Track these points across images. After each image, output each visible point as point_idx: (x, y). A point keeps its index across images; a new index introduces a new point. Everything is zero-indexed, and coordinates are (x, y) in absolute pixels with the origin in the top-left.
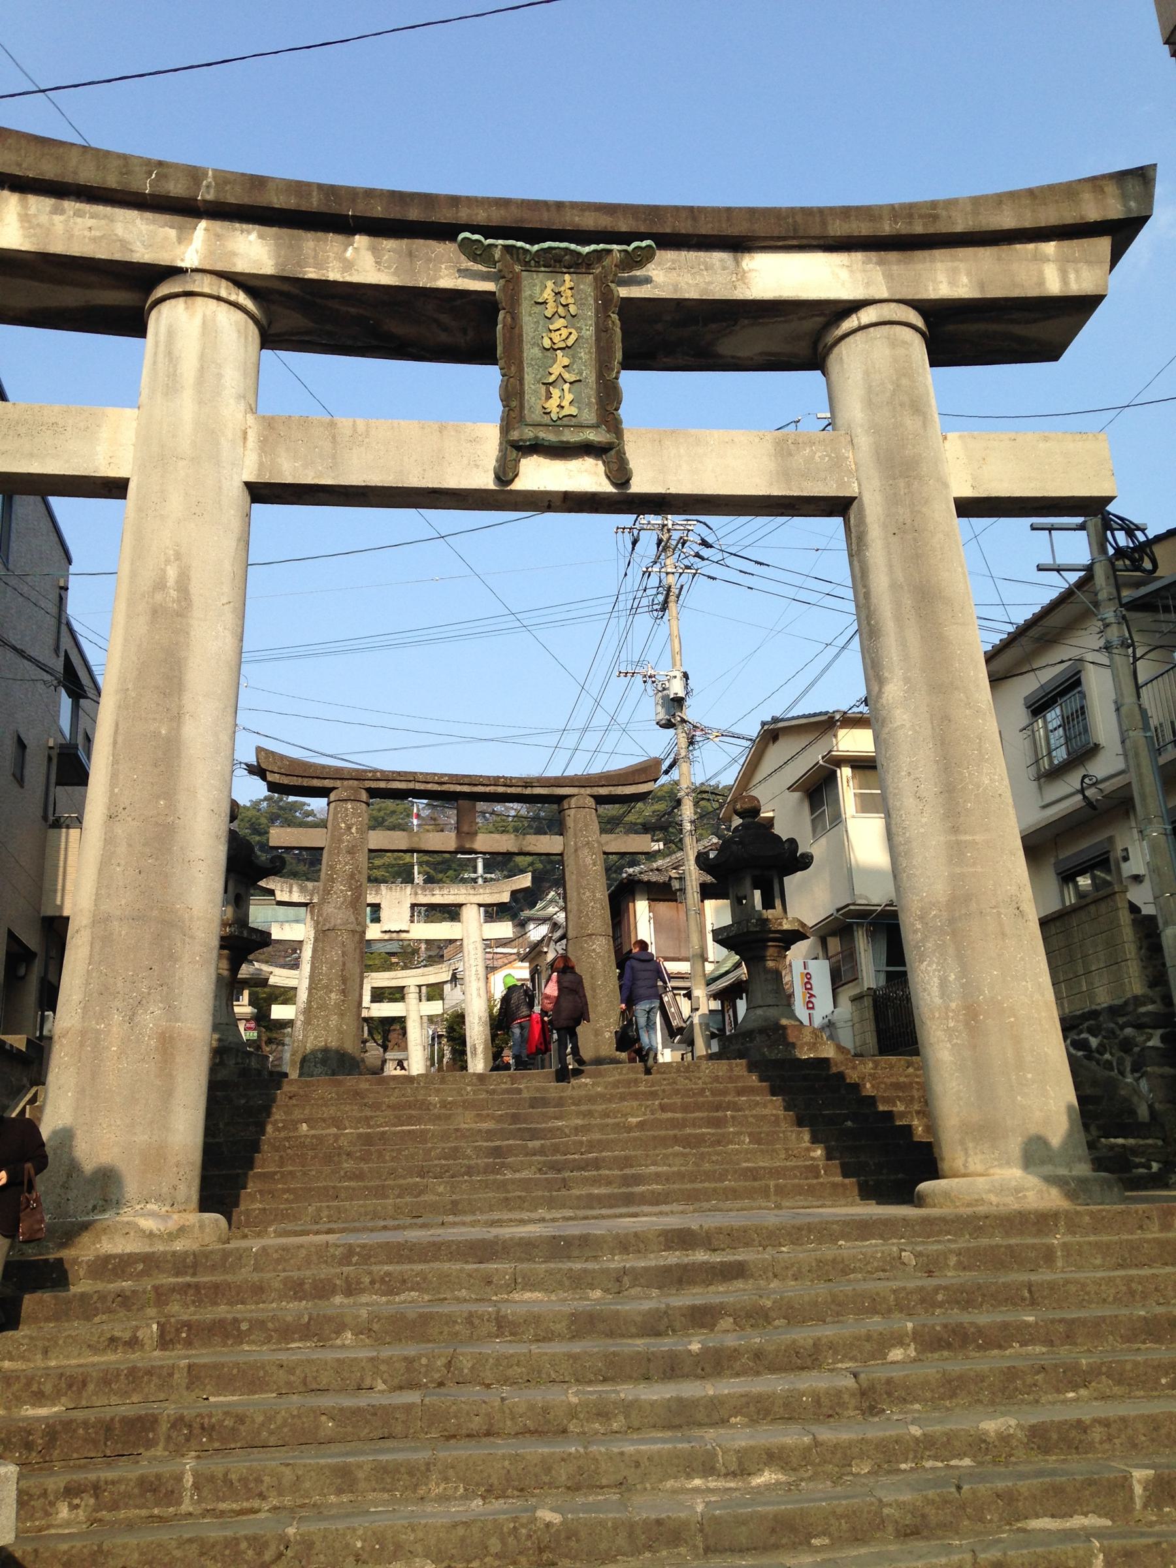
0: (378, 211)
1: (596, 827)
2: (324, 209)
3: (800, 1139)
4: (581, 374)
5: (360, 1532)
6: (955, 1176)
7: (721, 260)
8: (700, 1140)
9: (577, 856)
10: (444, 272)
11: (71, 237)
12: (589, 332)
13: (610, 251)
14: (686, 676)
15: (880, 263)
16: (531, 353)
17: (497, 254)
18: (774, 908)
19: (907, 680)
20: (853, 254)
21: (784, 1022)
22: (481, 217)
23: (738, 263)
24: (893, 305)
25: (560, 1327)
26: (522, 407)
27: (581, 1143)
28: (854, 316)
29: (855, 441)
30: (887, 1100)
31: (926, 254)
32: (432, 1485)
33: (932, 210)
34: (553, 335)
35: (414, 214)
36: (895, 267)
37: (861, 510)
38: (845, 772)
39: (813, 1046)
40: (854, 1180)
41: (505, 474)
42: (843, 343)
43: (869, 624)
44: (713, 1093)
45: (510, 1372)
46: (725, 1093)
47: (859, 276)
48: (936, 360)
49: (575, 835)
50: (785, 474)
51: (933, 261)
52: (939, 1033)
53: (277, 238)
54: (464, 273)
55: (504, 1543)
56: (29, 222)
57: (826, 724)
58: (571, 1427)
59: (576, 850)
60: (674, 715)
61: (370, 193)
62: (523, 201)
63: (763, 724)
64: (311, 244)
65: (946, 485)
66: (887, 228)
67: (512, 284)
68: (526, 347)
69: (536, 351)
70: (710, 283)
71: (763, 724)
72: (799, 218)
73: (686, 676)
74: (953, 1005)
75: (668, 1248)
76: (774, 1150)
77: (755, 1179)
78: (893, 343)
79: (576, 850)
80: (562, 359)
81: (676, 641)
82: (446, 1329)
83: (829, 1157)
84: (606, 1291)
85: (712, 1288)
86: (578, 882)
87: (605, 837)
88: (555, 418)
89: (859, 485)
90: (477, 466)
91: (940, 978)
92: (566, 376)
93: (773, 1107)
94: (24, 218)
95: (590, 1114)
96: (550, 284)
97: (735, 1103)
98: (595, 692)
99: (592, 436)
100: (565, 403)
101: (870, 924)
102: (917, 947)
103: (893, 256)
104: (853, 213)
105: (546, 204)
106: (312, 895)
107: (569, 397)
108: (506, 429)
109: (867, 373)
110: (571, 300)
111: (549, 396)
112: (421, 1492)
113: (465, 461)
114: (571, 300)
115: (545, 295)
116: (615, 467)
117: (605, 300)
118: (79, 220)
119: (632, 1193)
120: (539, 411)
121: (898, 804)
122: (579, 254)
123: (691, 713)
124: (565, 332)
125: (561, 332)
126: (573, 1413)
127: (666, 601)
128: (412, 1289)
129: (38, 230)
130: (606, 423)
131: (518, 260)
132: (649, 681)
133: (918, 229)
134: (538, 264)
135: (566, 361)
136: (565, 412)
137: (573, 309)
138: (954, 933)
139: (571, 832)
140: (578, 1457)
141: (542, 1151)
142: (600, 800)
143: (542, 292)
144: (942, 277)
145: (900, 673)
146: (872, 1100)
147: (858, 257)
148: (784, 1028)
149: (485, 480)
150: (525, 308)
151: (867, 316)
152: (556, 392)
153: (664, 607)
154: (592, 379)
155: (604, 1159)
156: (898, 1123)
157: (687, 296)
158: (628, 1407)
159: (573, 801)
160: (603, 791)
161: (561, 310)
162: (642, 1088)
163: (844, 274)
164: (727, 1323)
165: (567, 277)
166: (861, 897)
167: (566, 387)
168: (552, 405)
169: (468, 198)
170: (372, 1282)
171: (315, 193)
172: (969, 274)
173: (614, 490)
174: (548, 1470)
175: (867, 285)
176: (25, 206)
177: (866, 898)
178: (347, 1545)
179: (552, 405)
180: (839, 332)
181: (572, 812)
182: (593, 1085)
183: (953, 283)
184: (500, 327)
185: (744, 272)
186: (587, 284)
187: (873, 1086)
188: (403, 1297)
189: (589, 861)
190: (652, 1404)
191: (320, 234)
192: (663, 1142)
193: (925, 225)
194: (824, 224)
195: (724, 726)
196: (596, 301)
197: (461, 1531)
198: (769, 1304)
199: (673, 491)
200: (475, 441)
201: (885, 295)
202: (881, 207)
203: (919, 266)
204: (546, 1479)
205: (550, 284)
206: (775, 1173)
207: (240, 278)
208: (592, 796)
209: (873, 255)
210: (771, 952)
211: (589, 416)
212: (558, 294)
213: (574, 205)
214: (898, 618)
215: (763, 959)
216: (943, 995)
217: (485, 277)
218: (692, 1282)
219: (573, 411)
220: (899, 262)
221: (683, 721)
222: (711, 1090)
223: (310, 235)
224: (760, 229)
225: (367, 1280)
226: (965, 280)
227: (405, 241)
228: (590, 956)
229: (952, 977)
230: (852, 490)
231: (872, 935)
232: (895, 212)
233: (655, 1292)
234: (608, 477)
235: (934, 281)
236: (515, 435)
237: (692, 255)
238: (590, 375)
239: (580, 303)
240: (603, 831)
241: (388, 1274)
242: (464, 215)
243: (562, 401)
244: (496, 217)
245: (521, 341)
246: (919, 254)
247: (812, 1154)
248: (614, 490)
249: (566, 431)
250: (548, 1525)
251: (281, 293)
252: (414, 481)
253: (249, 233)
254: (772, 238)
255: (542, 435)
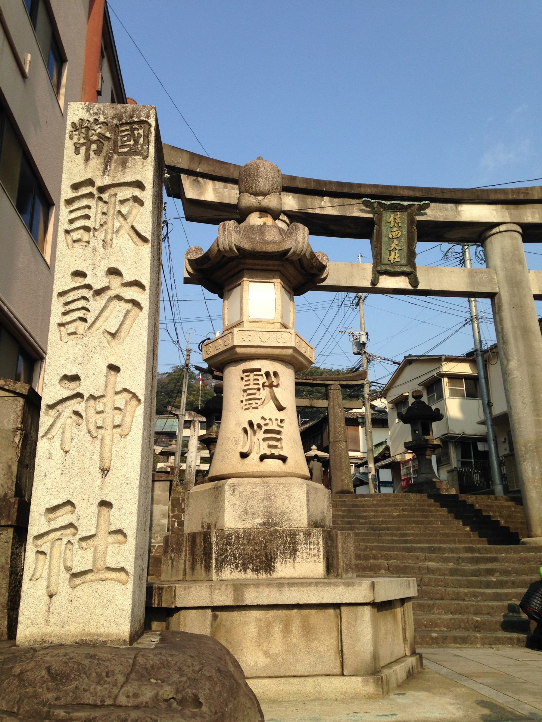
0: (334, 189)
1: (341, 397)
2: (316, 188)
3: (459, 524)
4: (401, 247)
5: (425, 619)
6: (537, 537)
7: (451, 207)
8: (422, 522)
9: (334, 409)
10: (355, 210)
11: (230, 197)
12: (405, 232)
13: (414, 205)
14: (367, 334)
15: (507, 209)
16: (385, 239)
17: (375, 205)
18: (429, 435)
19: (519, 361)
20: (498, 206)
21: (434, 480)
22: (368, 191)
23: (457, 208)
24: (512, 224)
25: (447, 572)
26: (381, 258)
27: (379, 521)
28: (497, 228)
29: (498, 272)
30: (486, 511)
31: (523, 206)
32: (435, 610)
33: (526, 191)
34: (393, 233)
35: (346, 190)
36: (512, 211)
37: (500, 298)
38: (445, 380)
39: (447, 490)
40: (486, 539)
41: (374, 282)
42: (492, 237)
43: (503, 339)
44: (419, 506)
45: (439, 584)
46: (424, 505)
47: (500, 213)
48: (524, 241)
49: (333, 401)
50: (472, 284)
51: (526, 209)
52: (531, 487)
53: (298, 198)
54: (362, 211)
55: (465, 625)
56: (216, 191)
57: (438, 360)
58: (466, 598)
59: (333, 406)
60: (361, 350)
61: (331, 182)
62: (383, 185)
63: (405, 357)
64: (310, 200)
65: (531, 290)
66: (510, 197)
67: (380, 215)
68: (383, 237)
69: (387, 239)
70: (448, 215)
71: (405, 357)
72: (479, 193)
73: (367, 334)
74: (537, 477)
75: (466, 552)
76: (452, 527)
77: (448, 537)
78: (512, 238)
79: (333, 406)
80: (396, 242)
81: (363, 319)
82: (412, 571)
83: (472, 530)
84: (454, 563)
85: (487, 564)
86: (334, 419)
87: (345, 402)
88: (392, 262)
89: (499, 289)
90: (364, 279)
91: (532, 468)
92: (397, 248)
93: (444, 511)
94: (215, 190)
95: (376, 511)
96: (392, 216)
97: (430, 510)
98: (332, 339)
99: (405, 269)
100: (396, 257)
101: (455, 442)
102: (522, 456)
103: (511, 206)
104: (498, 191)
105: (390, 187)
106: (194, 417)
107: (397, 255)
108: (375, 266)
109: (502, 249)
110: (399, 221)
111: (390, 255)
112: (432, 612)
113: (361, 277)
114: (399, 221)
115: (391, 219)
116: (413, 280)
117: (411, 222)
118: (233, 191)
119: (407, 540)
120: (387, 260)
121: (515, 405)
122: (403, 205)
123: (369, 349)
124: (397, 232)
125: (396, 232)
126: (466, 595)
127: (358, 302)
128: (394, 559)
129: (219, 194)
130: (410, 264)
131: (382, 207)
132: (351, 335)
133: (521, 197)
134: (389, 209)
135: (397, 243)
136: (396, 260)
137: (400, 224)
138: (537, 452)
139: (331, 399)
140: (475, 605)
141: (365, 523)
142: (342, 386)
143: (389, 219)
144: (529, 214)
145: (516, 358)
146: (480, 511)
147: (499, 206)
148: (435, 482)
149: (367, 284)
150: (383, 223)
151: (502, 228)
152: (393, 253)
153: (358, 304)
154: (405, 249)
155: (390, 527)
156: (492, 519)
157: (439, 220)
158: (482, 594)
159: (332, 387)
160: (344, 383)
161: (396, 225)
162: (391, 502)
163: (494, 213)
164: (497, 574)
165: (398, 213)
166: (451, 430)
167: (397, 251)
168: (391, 258)
169: (364, 184)
170: (382, 556)
171: (312, 182)
172: (539, 213)
173: (412, 288)
174: (468, 608)
175: (503, 217)
176: (215, 186)
177: (454, 431)
178: (422, 623)
179: (391, 258)
180: (491, 233)
181: (332, 391)
182: (373, 500)
183: (533, 217)
184: (375, 231)
185: (459, 211)
186: (405, 216)
187: (479, 506)
188: (392, 561)
189: (339, 411)
190: (489, 594)
191: (313, 196)
192: (409, 522)
193: (524, 196)
194: (488, 195)
195: (382, 356)
196: (408, 222)
197: (453, 621)
198: (510, 569)
199: (433, 289)
200: (363, 269)
201: (509, 221)
202: (508, 189)
203: (521, 210)
204: (467, 611)
205: (392, 216)
206: (455, 535)
207: (288, 213)
208: (340, 385)
209: (505, 206)
210: (428, 452)
211: (404, 262)
212: (395, 219)
213: (401, 187)
214: (515, 338)
215: (425, 455)
216: (533, 474)
217: (369, 212)
218: (481, 562)
219: (399, 260)
220: (514, 209)
221: (365, 352)
222: (418, 504)
223: (309, 197)
224: (465, 196)
225: (380, 555)
226: (537, 216)
227: (341, 199)
228: (339, 450)
229: (537, 468)
230: (496, 290)
231: (456, 447)
232: (513, 191)
233: (469, 565)
234: (410, 283)
235: (526, 216)
236: (379, 268)
237: (441, 205)
238: (405, 247)
239: (402, 222)
240: (344, 399)
241: (386, 554)
242: (362, 191)
243: (395, 257)
244: (374, 191)
245: (382, 235)
246: (521, 206)
247: (466, 529)
248: (412, 288)
249: (396, 267)
250: (477, 621)
251: (298, 216)
252: (343, 284)
253: (289, 196)
254: (470, 200)
255: (388, 268)
